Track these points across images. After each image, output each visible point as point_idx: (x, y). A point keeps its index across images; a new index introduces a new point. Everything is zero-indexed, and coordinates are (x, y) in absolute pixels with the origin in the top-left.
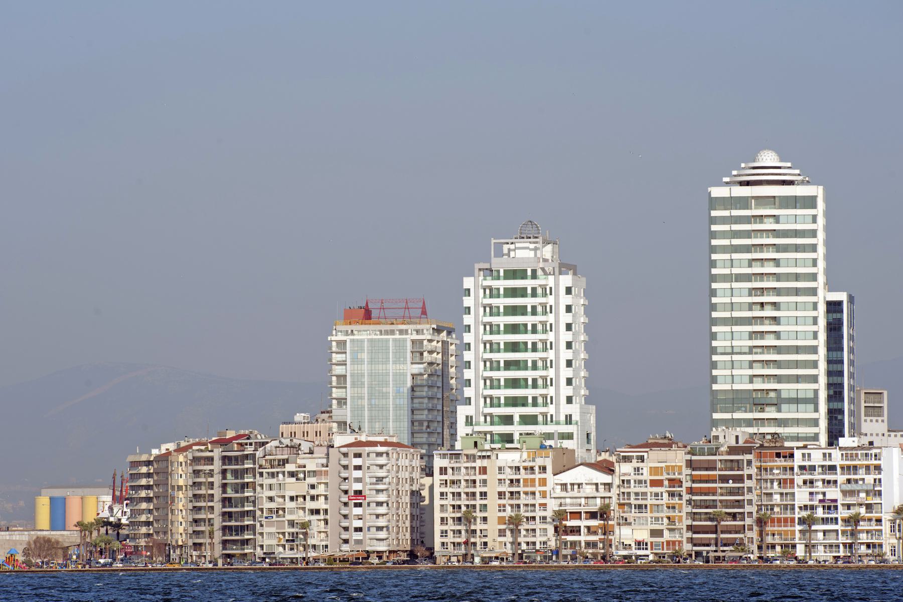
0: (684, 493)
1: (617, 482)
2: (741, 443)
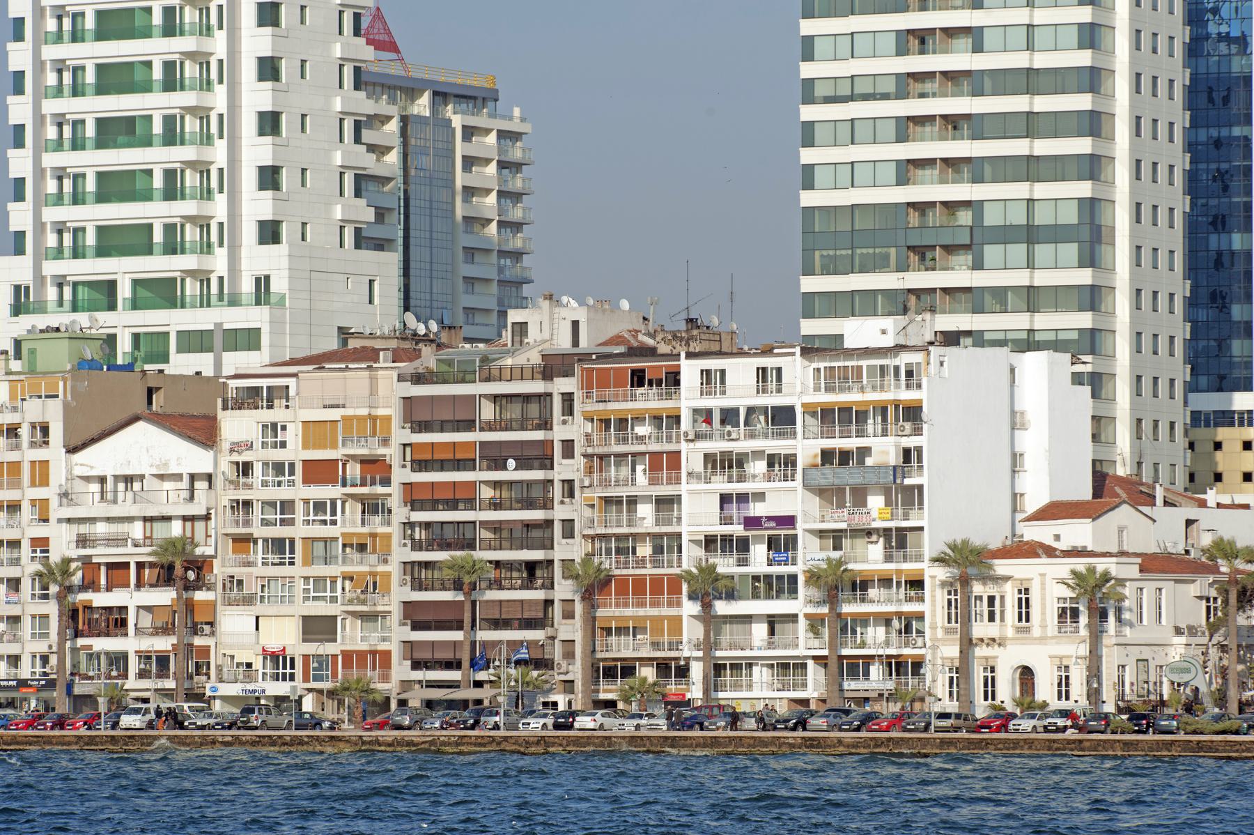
0: (395, 502)
1: (225, 466)
2: (584, 343)
